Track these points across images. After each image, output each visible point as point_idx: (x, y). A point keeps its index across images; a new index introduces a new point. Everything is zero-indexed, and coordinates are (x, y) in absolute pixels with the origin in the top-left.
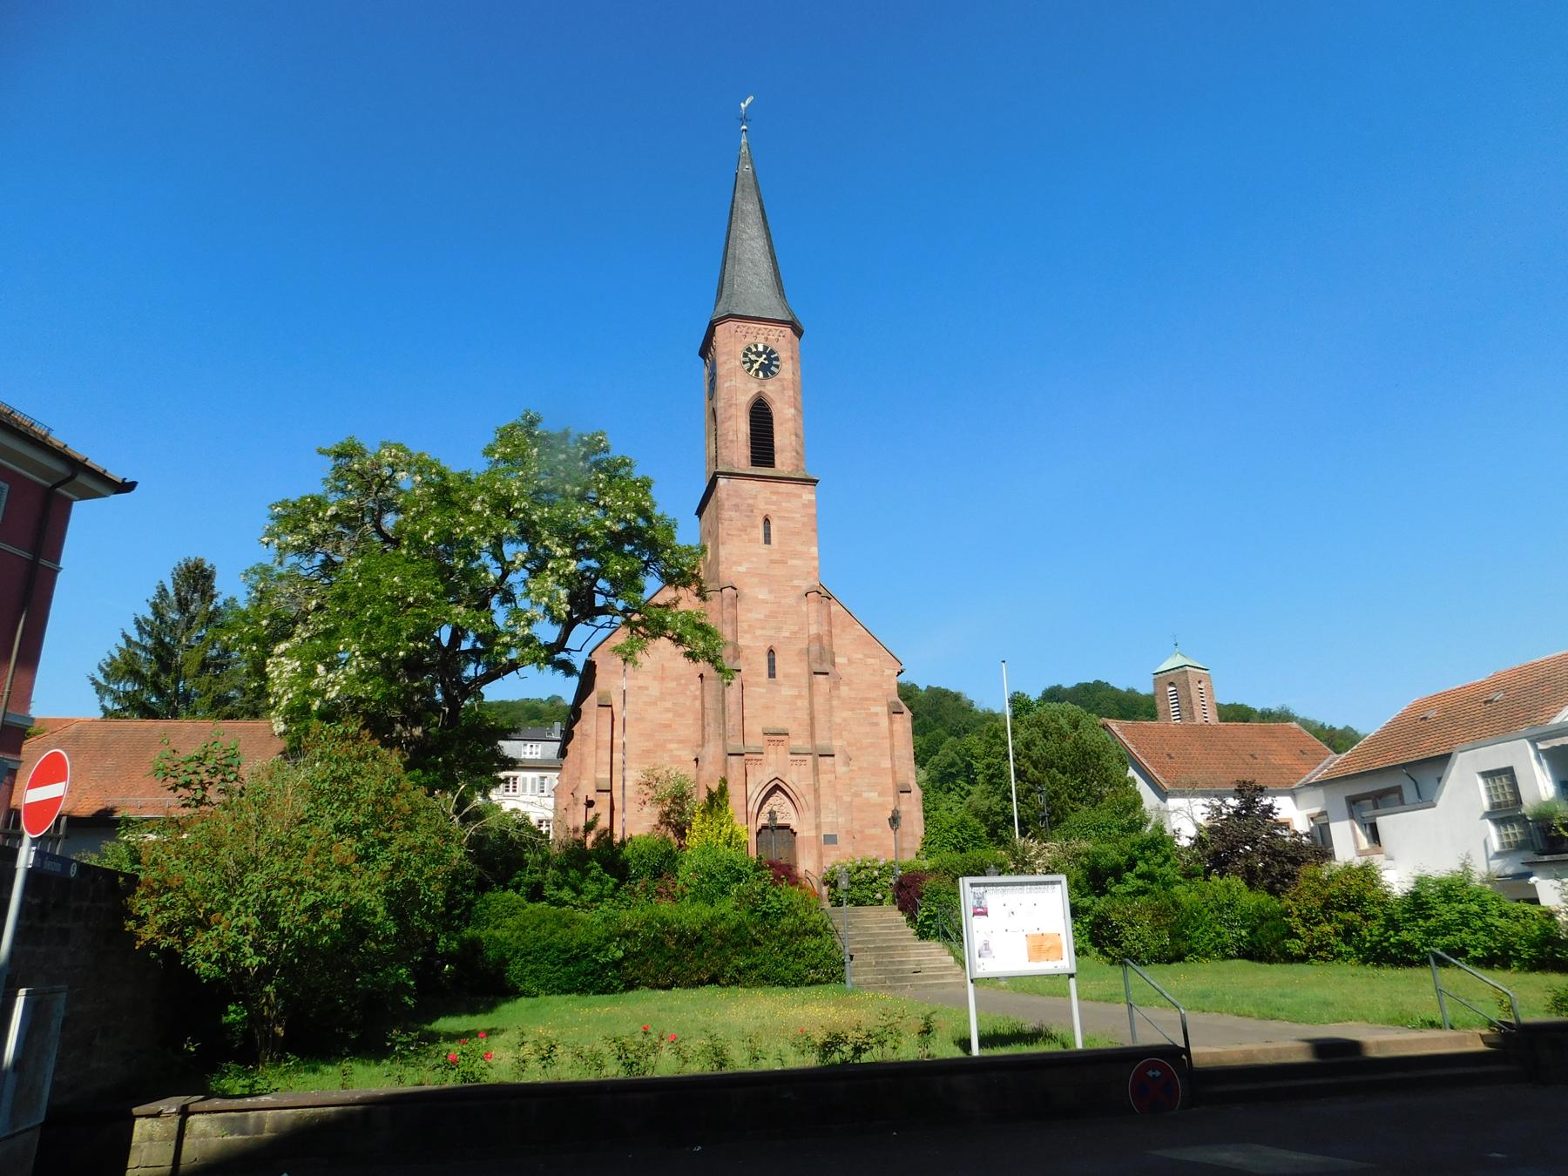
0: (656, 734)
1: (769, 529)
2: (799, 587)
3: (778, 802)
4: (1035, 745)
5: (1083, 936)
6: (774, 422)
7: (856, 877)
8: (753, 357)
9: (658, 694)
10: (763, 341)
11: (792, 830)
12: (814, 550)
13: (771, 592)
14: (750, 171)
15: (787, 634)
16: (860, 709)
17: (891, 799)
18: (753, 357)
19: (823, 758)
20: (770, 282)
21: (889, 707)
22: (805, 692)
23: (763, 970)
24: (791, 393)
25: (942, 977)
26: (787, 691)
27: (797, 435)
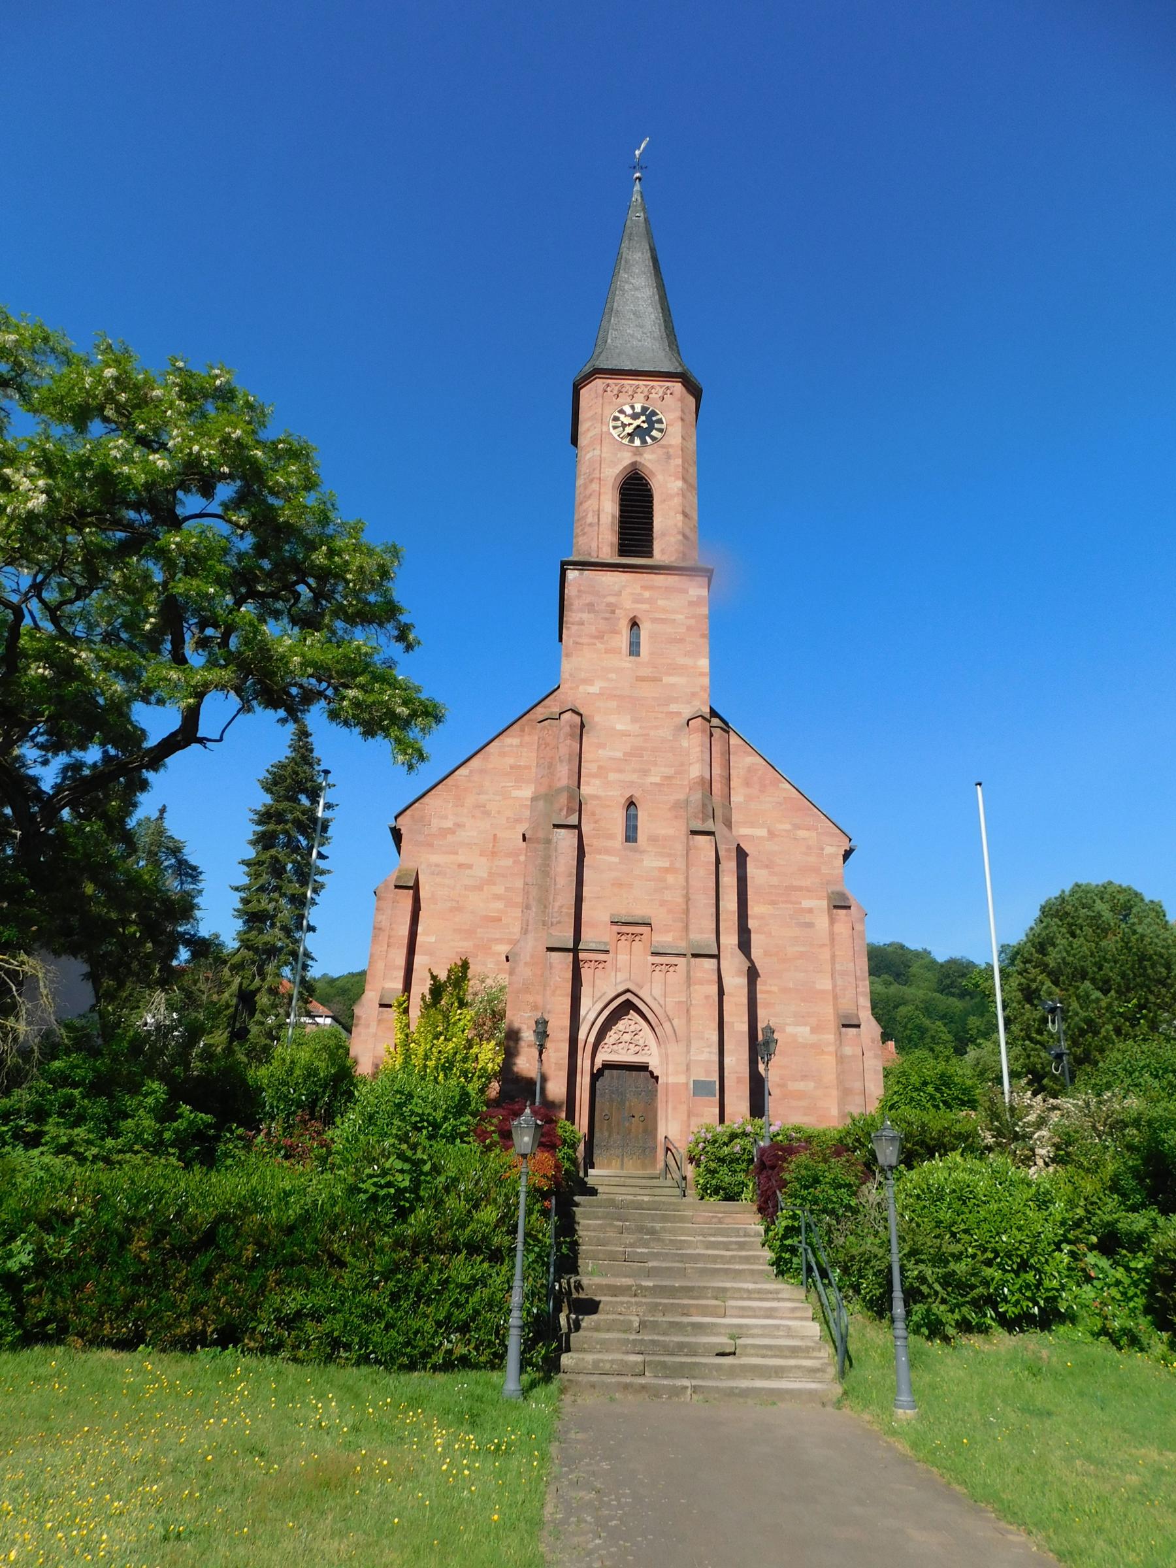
0: (479, 930)
1: (638, 636)
2: (679, 714)
3: (632, 1028)
4: (1054, 945)
5: (1131, 1299)
6: (655, 502)
7: (726, 1150)
8: (627, 420)
9: (485, 875)
10: (643, 400)
11: (652, 1073)
12: (704, 663)
13: (635, 720)
14: (642, 219)
15: (657, 780)
16: (786, 902)
17: (831, 1037)
18: (627, 420)
19: (698, 960)
20: (657, 333)
21: (829, 898)
22: (680, 864)
23: (333, 1324)
24: (679, 461)
25: (778, 1372)
26: (651, 862)
27: (685, 514)
